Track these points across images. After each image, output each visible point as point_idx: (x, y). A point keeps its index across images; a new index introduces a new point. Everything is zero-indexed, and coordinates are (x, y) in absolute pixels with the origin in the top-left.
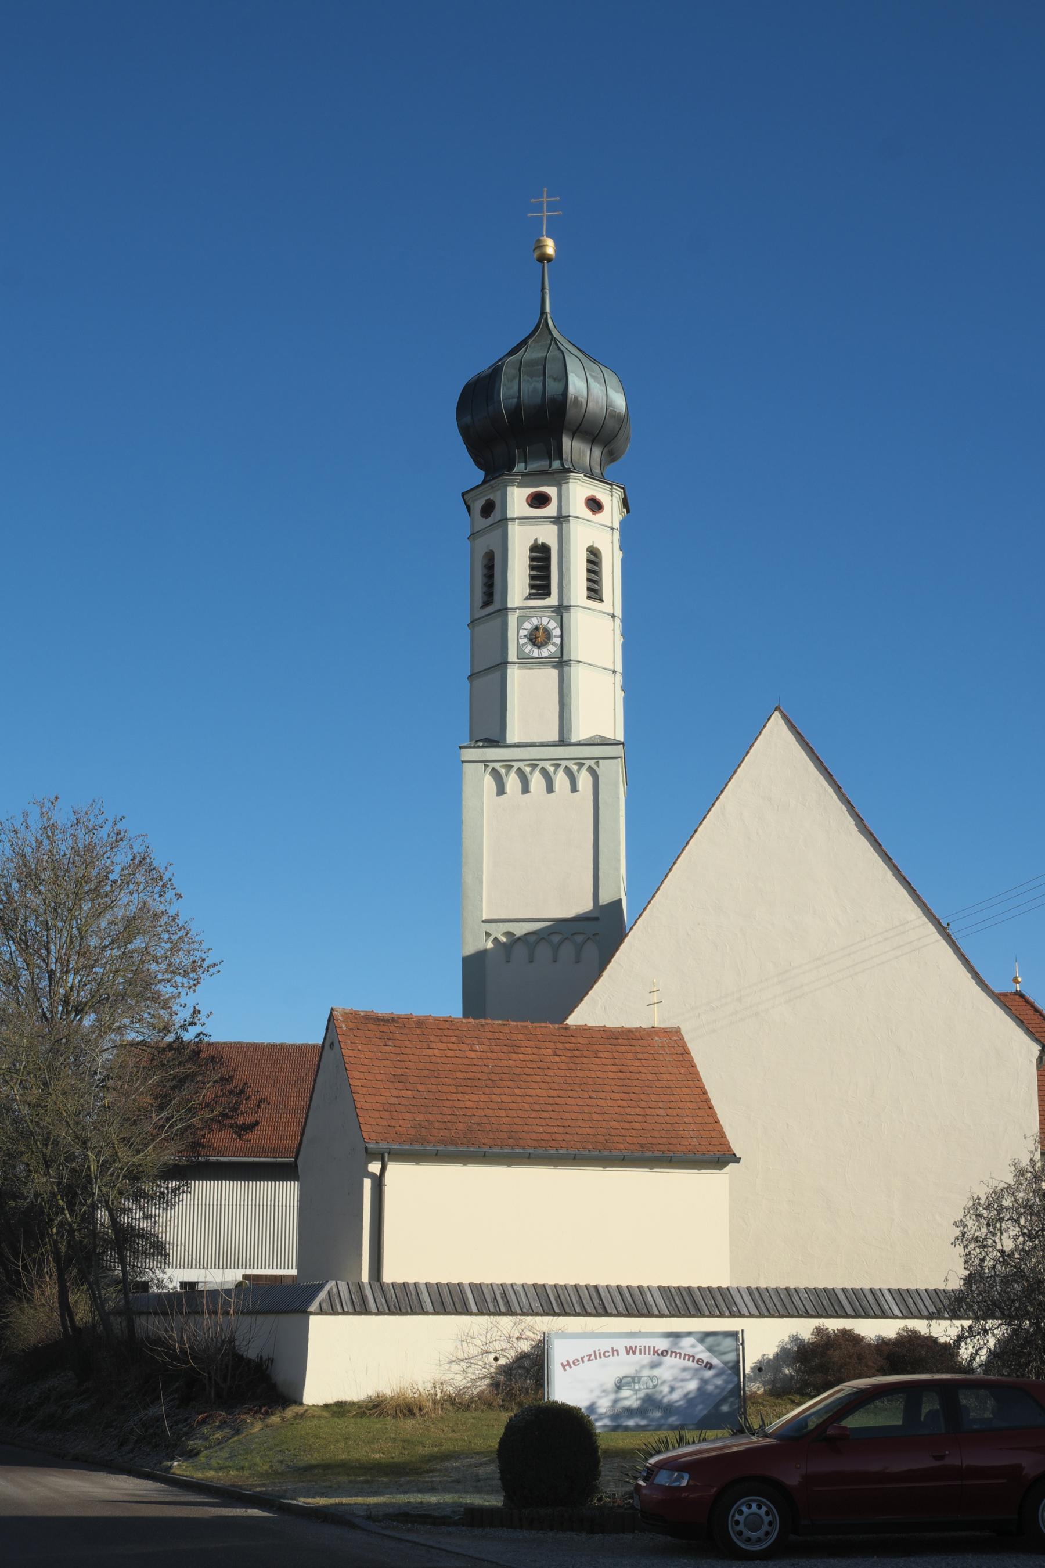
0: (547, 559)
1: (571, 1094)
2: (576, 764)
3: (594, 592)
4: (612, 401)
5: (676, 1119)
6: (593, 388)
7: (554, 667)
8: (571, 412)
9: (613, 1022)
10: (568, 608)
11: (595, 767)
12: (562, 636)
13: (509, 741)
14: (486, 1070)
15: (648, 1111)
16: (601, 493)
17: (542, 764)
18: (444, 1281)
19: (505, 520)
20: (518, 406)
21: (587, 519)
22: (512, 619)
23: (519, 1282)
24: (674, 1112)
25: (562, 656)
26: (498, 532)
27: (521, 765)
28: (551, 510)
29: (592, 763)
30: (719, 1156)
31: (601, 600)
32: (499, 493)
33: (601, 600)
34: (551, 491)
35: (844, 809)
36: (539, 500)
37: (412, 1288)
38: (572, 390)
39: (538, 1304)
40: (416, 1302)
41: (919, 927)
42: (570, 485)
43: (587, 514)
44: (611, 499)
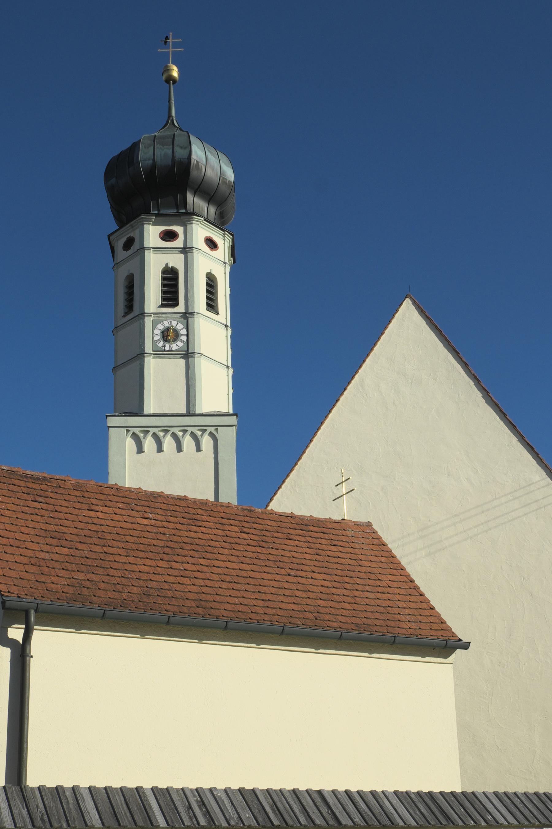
0: (176, 279)
1: (266, 569)
2: (199, 430)
3: (212, 305)
4: (224, 171)
5: (388, 603)
6: (211, 162)
7: (182, 358)
8: (194, 173)
9: (302, 511)
10: (193, 314)
11: (215, 433)
12: (187, 335)
13: (146, 412)
14: (162, 537)
15: (357, 593)
16: (217, 236)
17: (172, 430)
18: (116, 785)
19: (142, 249)
20: (153, 165)
21: (206, 254)
22: (148, 322)
23: (221, 786)
24: (385, 596)
25: (188, 350)
26: (137, 259)
27: (156, 430)
28: (179, 243)
29: (212, 429)
30: (441, 643)
31: (217, 313)
32: (137, 231)
33: (217, 313)
34: (179, 229)
35: (472, 383)
36: (169, 236)
37: (68, 794)
38: (194, 157)
39: (248, 814)
40: (74, 813)
41: (543, 487)
42: (194, 226)
43: (206, 249)
44: (224, 242)
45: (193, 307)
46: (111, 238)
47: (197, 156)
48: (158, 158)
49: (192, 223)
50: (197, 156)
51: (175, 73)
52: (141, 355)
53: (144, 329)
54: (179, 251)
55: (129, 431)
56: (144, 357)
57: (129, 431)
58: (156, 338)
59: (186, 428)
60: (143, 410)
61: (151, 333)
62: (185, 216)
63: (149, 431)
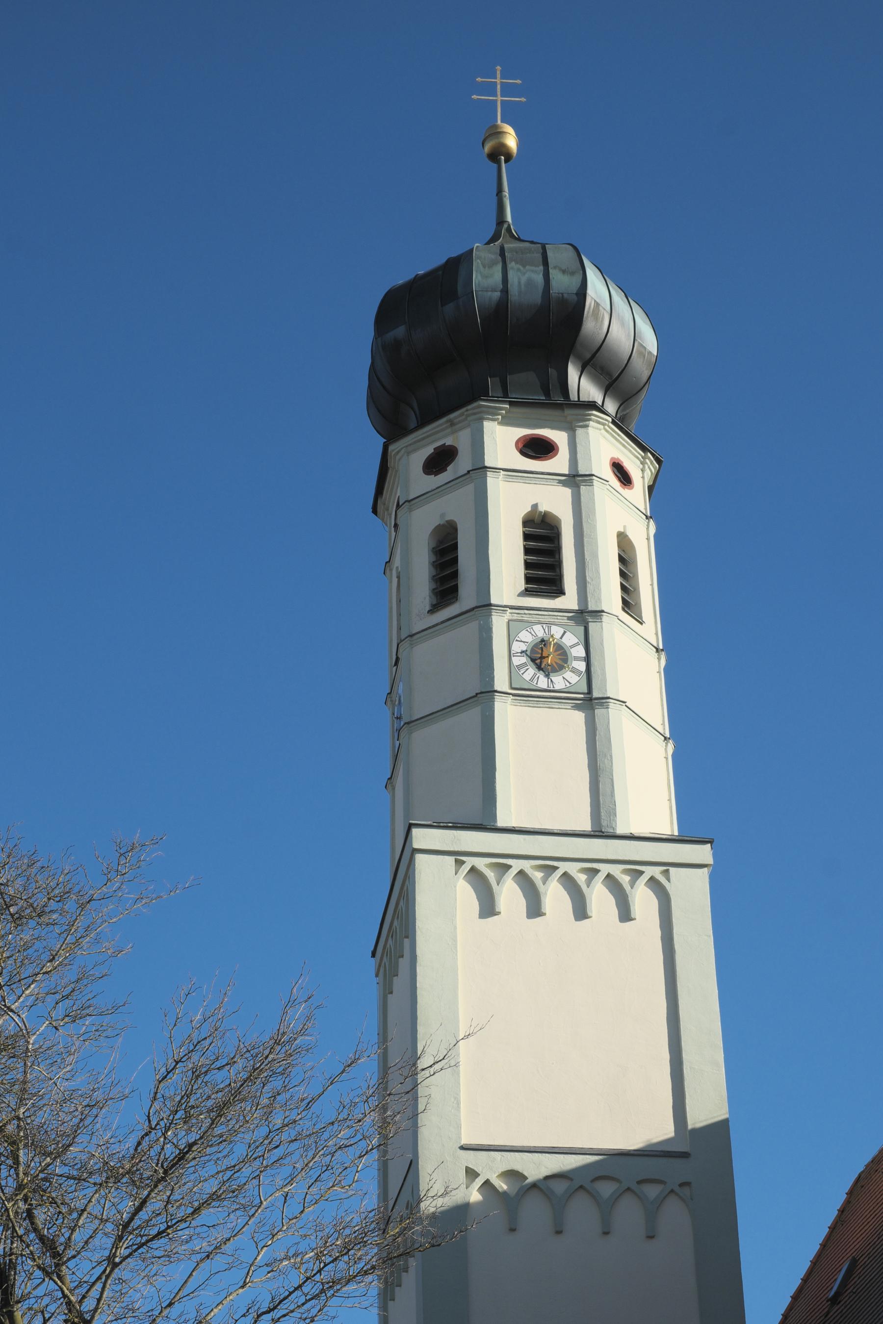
2: (626, 872)
3: (630, 604)
7: (577, 707)
8: (589, 325)
11: (662, 879)
12: (588, 659)
17: (564, 867)
19: (480, 470)
22: (499, 623)
28: (559, 463)
34: (559, 437)
36: (537, 448)
44: (641, 471)
45: (599, 600)
46: (391, 448)
47: (596, 292)
48: (514, 289)
49: (587, 426)
50: (596, 292)
51: (511, 141)
52: (486, 694)
54: (560, 482)
55: (463, 862)
56: (492, 700)
57: (463, 862)
58: (517, 661)
59: (555, 864)
63: (510, 867)
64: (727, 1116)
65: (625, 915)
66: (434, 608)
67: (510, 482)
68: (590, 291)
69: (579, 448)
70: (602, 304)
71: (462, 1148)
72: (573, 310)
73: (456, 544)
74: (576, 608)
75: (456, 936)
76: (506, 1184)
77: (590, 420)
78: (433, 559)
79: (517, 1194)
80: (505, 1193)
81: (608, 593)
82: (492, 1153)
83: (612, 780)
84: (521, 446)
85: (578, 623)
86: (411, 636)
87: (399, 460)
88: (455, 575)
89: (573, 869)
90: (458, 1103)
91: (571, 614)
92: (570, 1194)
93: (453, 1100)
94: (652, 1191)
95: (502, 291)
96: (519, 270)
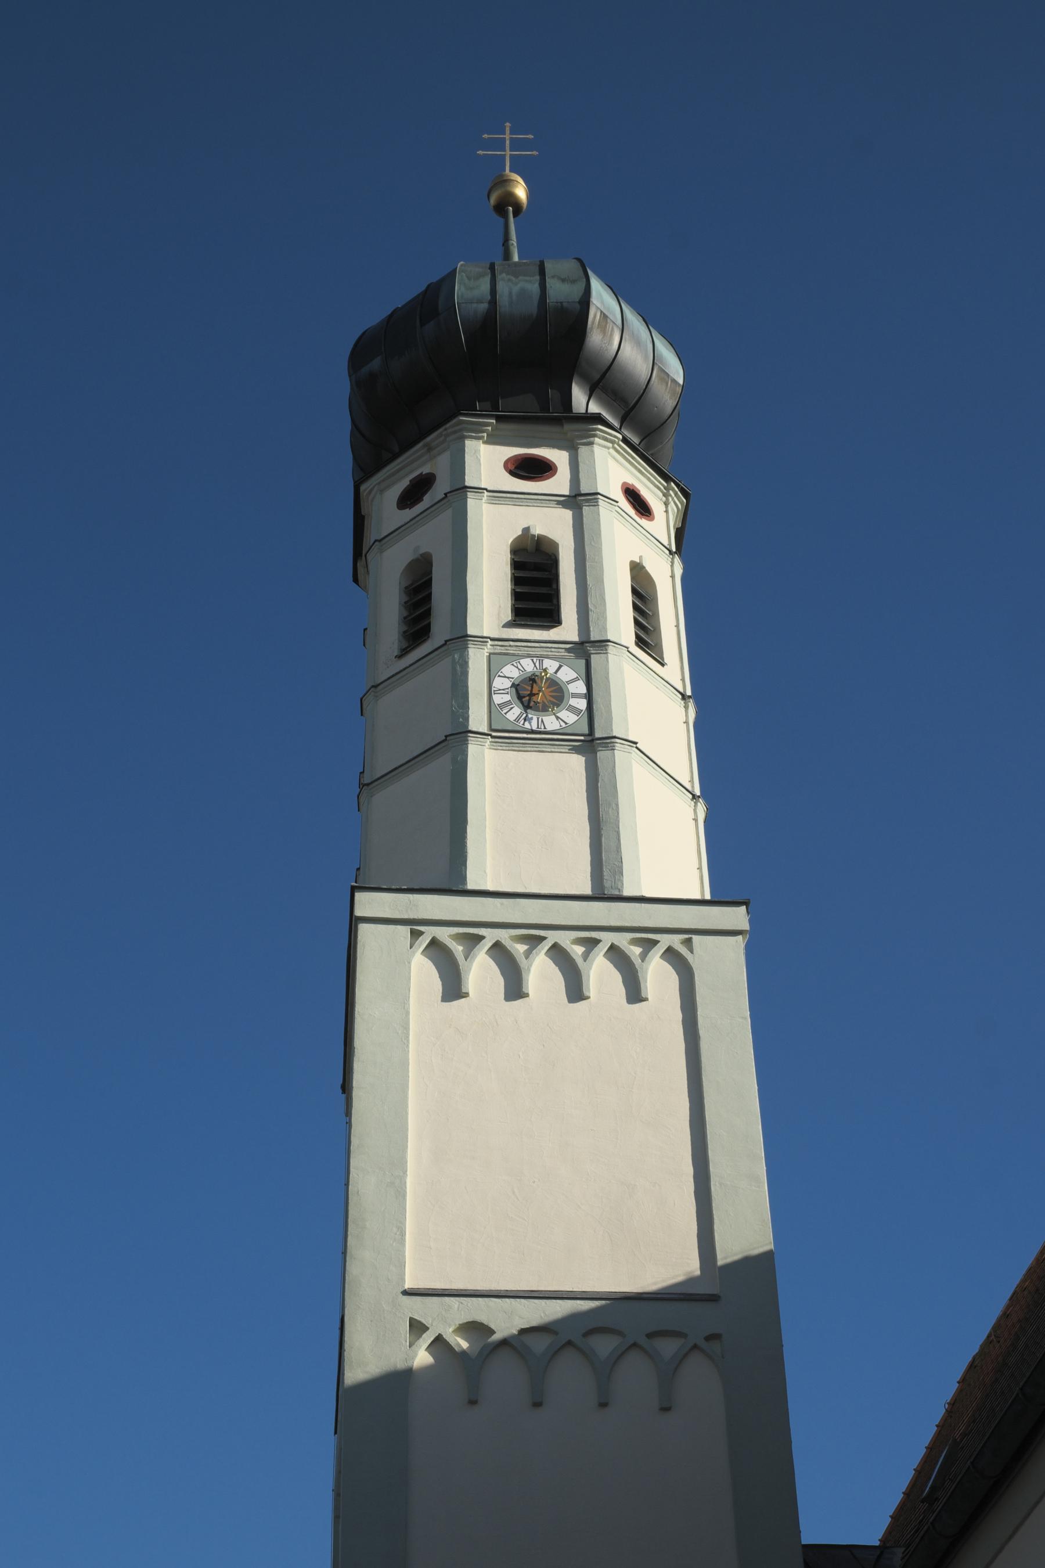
2: (635, 942)
3: (647, 637)
6: (625, 337)
7: (576, 750)
8: (595, 338)
11: (683, 950)
12: (589, 696)
16: (651, 491)
17: (553, 937)
22: (477, 659)
27: (503, 936)
28: (559, 483)
29: (675, 941)
34: (559, 457)
36: (532, 469)
45: (604, 629)
46: (362, 488)
49: (592, 443)
51: (521, 192)
52: (459, 735)
53: (465, 674)
54: (559, 503)
55: (421, 933)
56: (465, 743)
57: (421, 933)
58: (498, 699)
59: (542, 933)
60: (463, 879)
61: (486, 687)
62: (572, 430)
63: (482, 938)
64: (772, 1247)
65: (635, 994)
66: (403, 653)
67: (495, 502)
68: (595, 300)
69: (582, 467)
70: (610, 316)
71: (406, 1293)
72: (575, 320)
73: (431, 579)
74: (576, 639)
75: (408, 1023)
76: (466, 1340)
77: (595, 436)
78: (405, 598)
79: (481, 1352)
80: (464, 1353)
81: (619, 621)
82: (447, 1299)
83: (618, 833)
84: (512, 468)
85: (578, 657)
86: (375, 687)
87: (372, 501)
88: (428, 613)
89: (565, 939)
90: (403, 1234)
91: (568, 646)
92: (555, 1352)
93: (395, 1230)
94: (668, 1348)
95: (490, 302)
96: (509, 280)
